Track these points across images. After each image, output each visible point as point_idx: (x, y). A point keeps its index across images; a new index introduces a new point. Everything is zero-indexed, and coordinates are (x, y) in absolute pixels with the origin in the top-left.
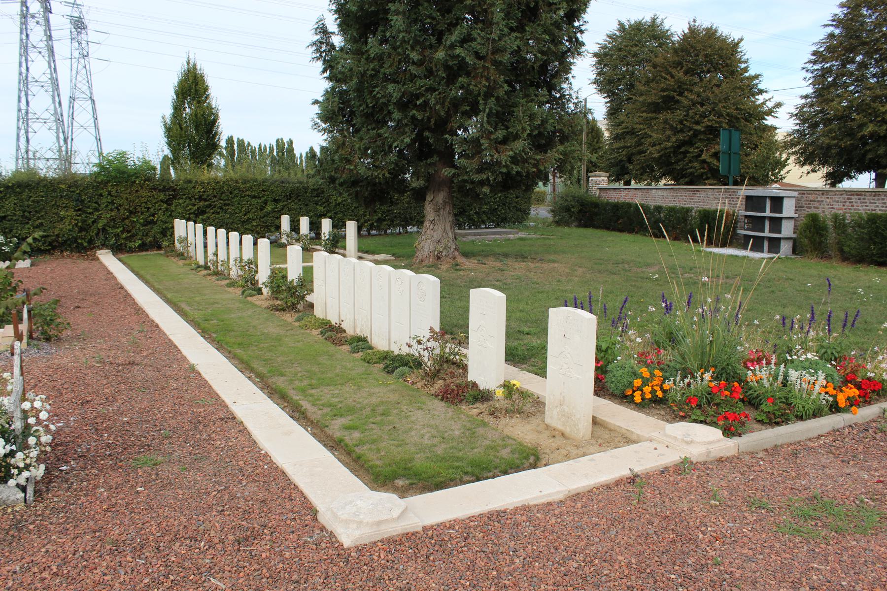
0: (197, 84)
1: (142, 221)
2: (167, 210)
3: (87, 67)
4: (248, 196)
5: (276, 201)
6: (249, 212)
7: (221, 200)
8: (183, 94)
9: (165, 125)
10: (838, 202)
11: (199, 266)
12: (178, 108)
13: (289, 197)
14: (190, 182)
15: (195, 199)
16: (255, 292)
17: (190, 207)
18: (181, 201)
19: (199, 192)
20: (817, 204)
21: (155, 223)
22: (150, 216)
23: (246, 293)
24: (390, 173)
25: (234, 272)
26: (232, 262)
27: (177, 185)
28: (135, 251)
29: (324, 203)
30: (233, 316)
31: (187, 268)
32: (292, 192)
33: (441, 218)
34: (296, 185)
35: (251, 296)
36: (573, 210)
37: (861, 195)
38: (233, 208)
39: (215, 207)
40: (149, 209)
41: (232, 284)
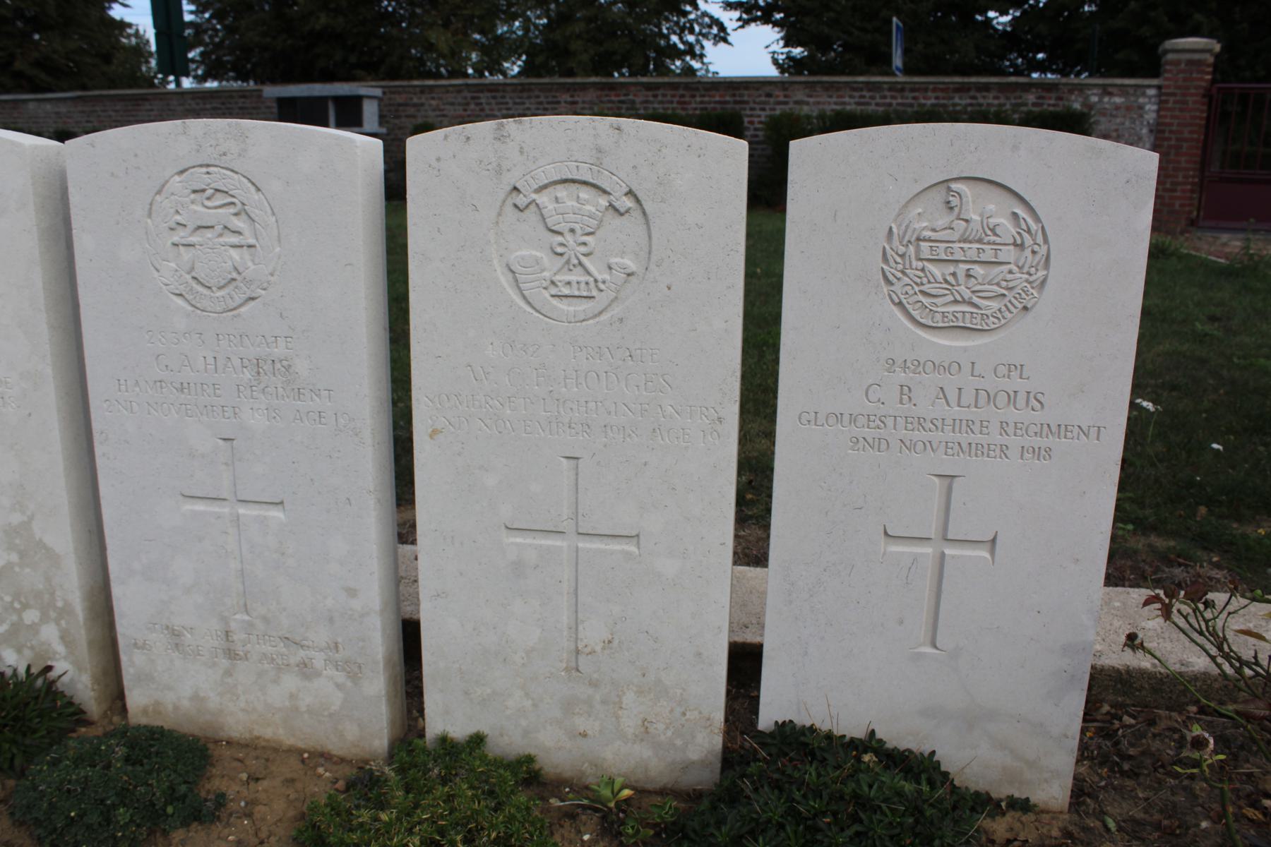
10: (453, 104)
20: (411, 111)
33: (1188, 194)
37: (497, 91)
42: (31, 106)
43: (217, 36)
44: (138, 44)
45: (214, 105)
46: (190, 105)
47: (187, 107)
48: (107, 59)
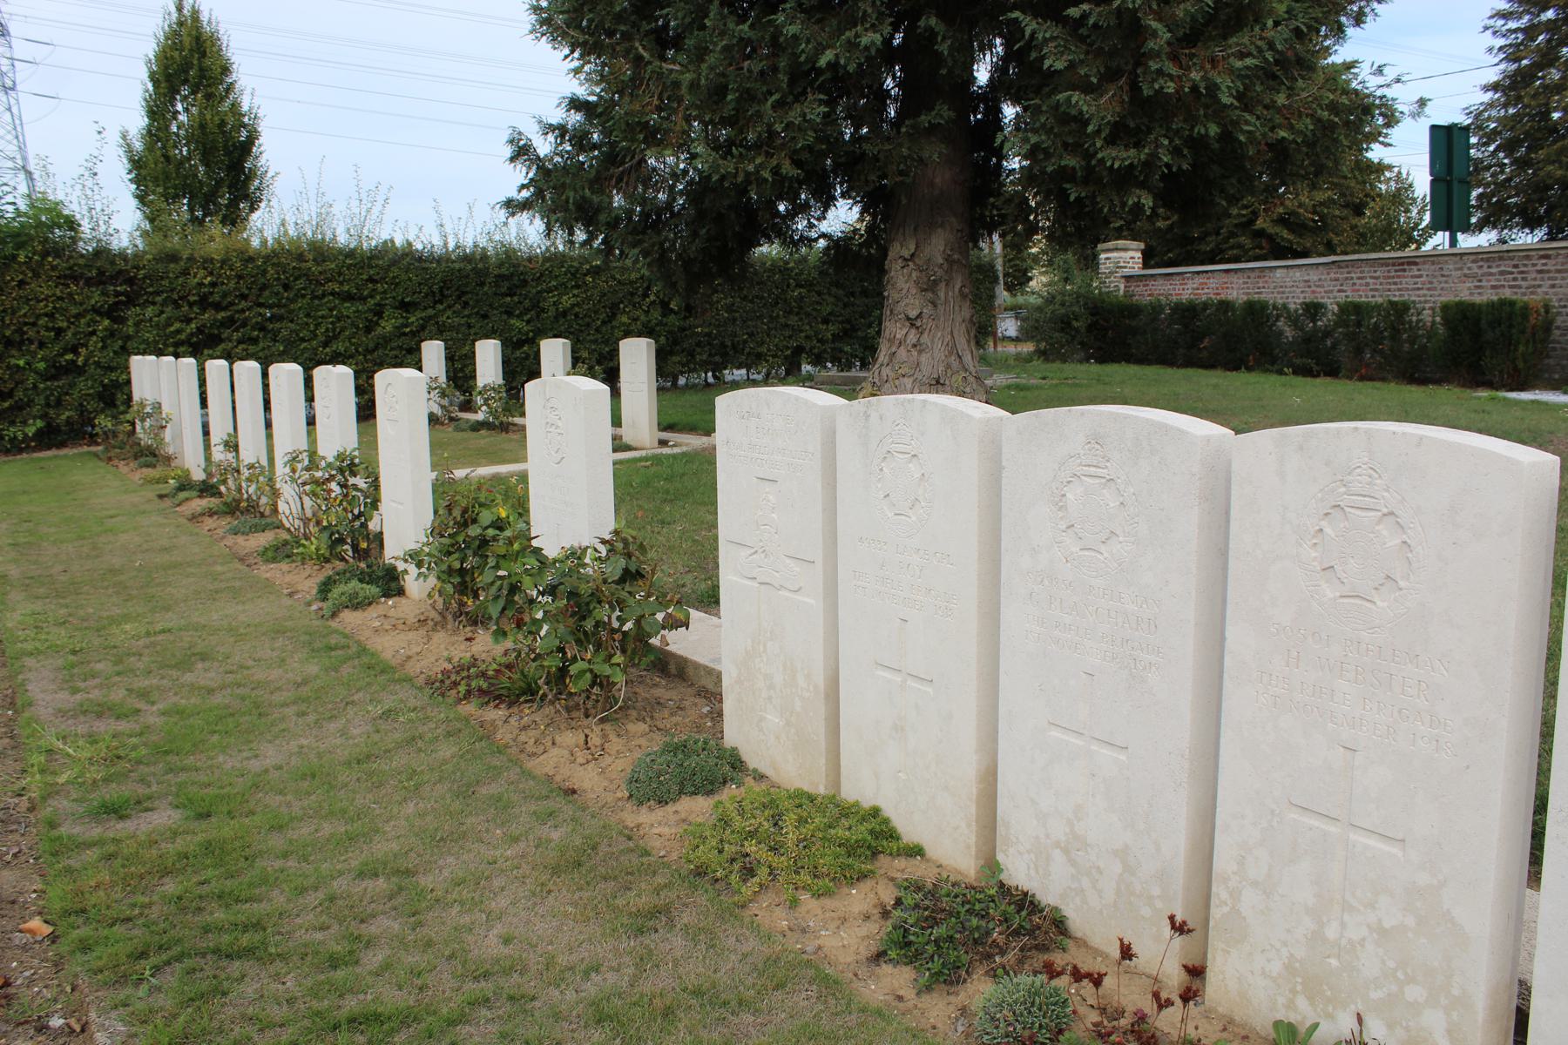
0: (203, 54)
1: (42, 366)
2: (112, 334)
3: (15, 110)
4: (333, 294)
5: (405, 306)
6: (336, 337)
7: (260, 305)
8: (169, 77)
9: (129, 150)
11: (185, 485)
12: (158, 111)
13: (439, 297)
14: (173, 257)
15: (191, 305)
16: (373, 590)
17: (177, 325)
18: (150, 311)
19: (201, 284)
21: (80, 371)
22: (66, 351)
23: (336, 591)
24: (797, 163)
25: (291, 504)
26: (281, 470)
27: (138, 268)
28: (28, 449)
29: (527, 310)
30: (272, 754)
31: (151, 492)
32: (446, 284)
33: (941, 309)
34: (457, 266)
35: (357, 604)
36: (1075, 324)
38: (292, 326)
39: (244, 325)
40: (59, 332)
41: (280, 552)
42: (1279, 273)
43: (1502, 172)
44: (1398, 190)
45: (1503, 268)
46: (1469, 269)
47: (1466, 271)
48: (1358, 210)
